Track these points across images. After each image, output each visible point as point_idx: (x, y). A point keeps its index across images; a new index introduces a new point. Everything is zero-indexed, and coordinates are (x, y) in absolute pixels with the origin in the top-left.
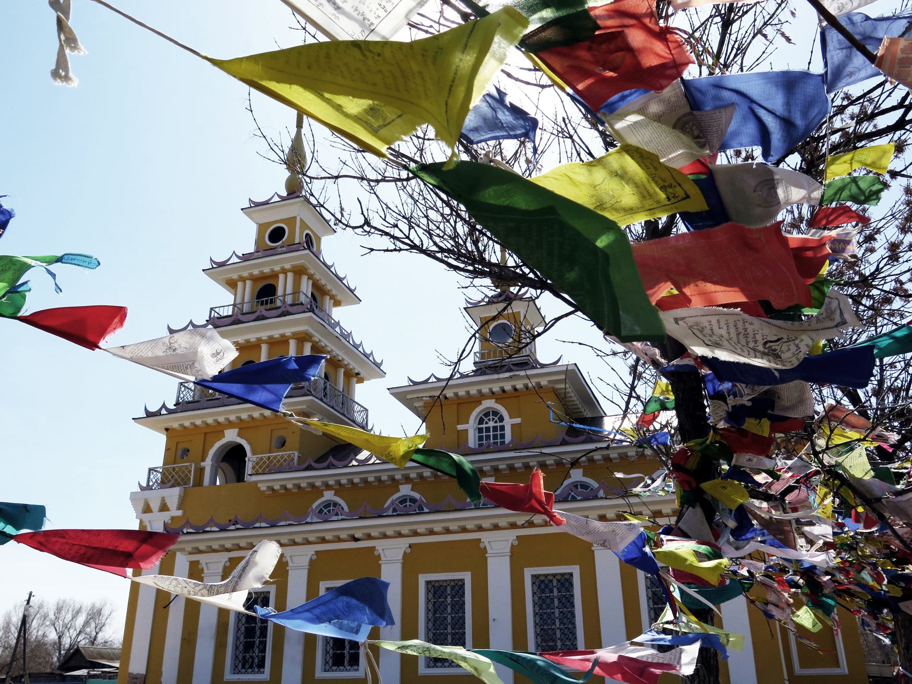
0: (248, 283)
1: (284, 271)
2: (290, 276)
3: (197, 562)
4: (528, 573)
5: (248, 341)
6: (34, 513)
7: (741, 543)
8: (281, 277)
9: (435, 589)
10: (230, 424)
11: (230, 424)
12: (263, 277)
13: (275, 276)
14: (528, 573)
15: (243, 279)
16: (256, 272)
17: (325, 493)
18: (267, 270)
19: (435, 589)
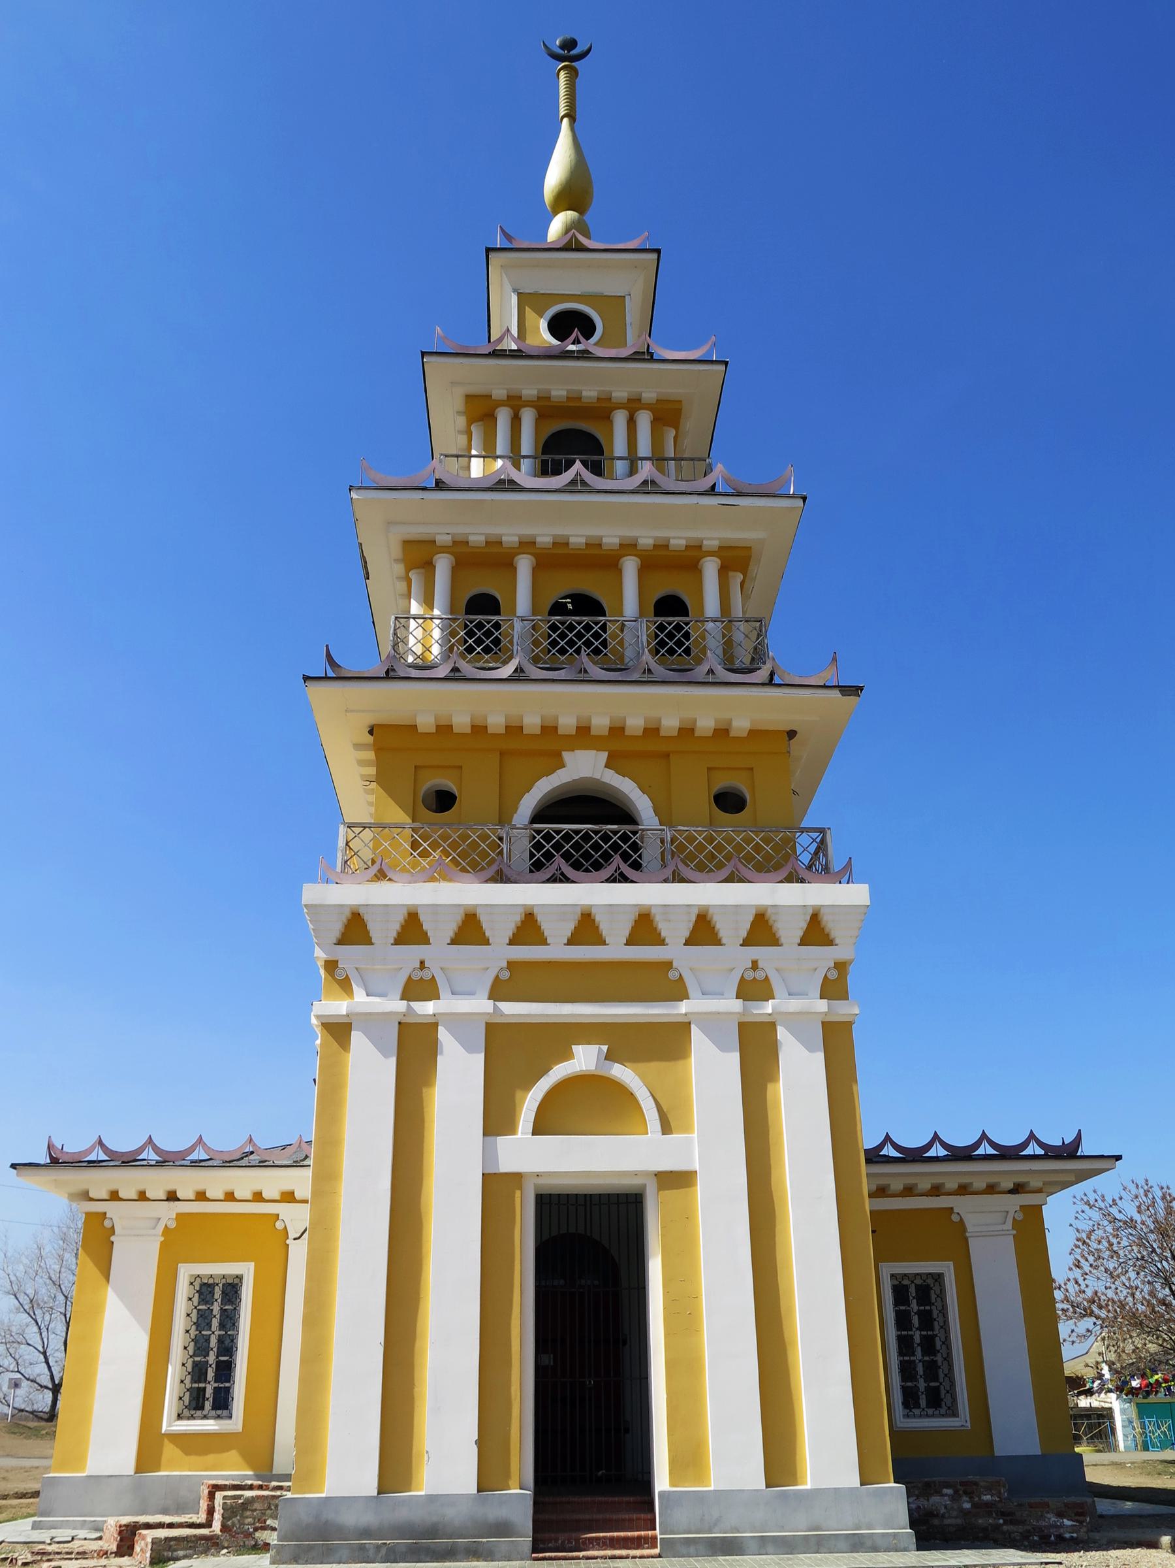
0: (528, 418)
1: (633, 406)
2: (644, 420)
3: (308, 1203)
4: (186, 1272)
5: (561, 543)
6: (368, 579)
7: (930, 1281)
8: (620, 419)
9: (205, 1290)
10: (583, 736)
11: (583, 736)
12: (574, 408)
13: (603, 411)
14: (186, 1272)
15: (515, 403)
16: (559, 393)
17: (578, 1050)
18: (590, 393)
19: (205, 1290)
